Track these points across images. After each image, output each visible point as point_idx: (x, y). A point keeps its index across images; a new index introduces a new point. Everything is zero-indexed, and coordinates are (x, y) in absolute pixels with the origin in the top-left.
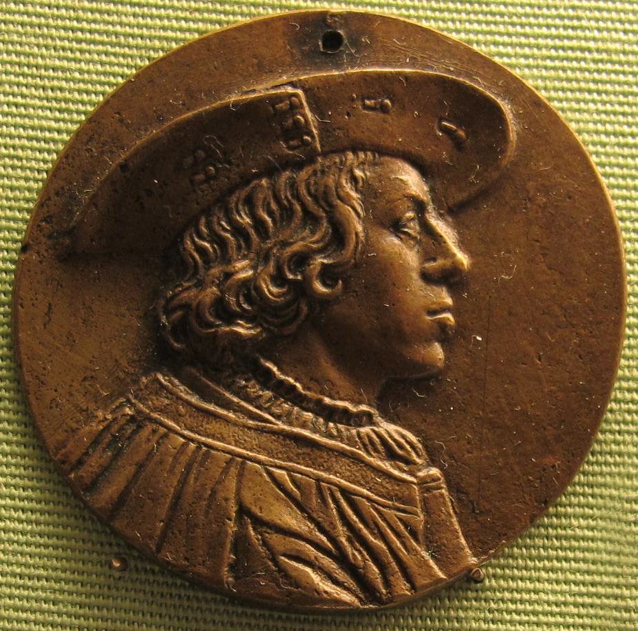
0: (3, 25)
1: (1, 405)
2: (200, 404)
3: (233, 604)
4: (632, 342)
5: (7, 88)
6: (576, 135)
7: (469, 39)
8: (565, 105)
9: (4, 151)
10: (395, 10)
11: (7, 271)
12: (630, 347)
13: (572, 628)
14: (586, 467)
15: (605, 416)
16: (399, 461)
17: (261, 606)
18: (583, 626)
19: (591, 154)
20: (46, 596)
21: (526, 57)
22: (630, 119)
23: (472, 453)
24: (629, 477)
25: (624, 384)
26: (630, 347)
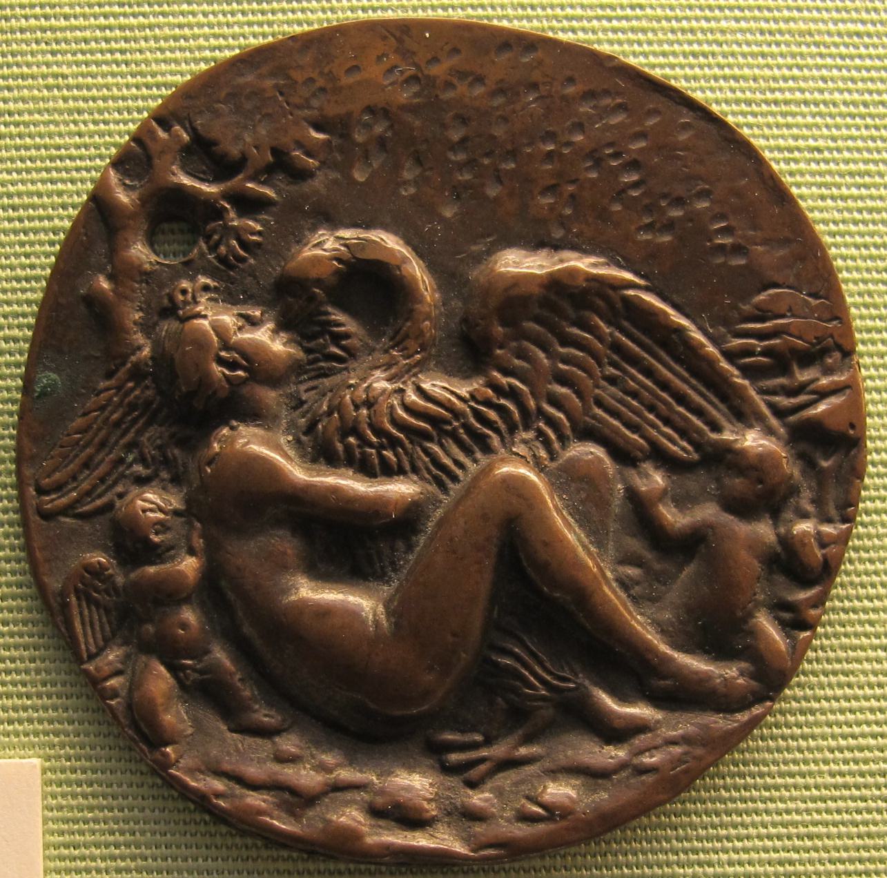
0: (3, 21)
2: (340, 597)
3: (266, 847)
4: (879, 444)
6: (807, 213)
7: (846, 782)
8: (750, 119)
10: (470, 11)
12: (878, 451)
13: (863, 876)
14: (806, 665)
16: (605, 691)
17: (284, 846)
18: (867, 873)
19: (824, 233)
20: (785, 870)
21: (854, 799)
22: (877, 603)
23: (396, 364)
26: (878, 451)
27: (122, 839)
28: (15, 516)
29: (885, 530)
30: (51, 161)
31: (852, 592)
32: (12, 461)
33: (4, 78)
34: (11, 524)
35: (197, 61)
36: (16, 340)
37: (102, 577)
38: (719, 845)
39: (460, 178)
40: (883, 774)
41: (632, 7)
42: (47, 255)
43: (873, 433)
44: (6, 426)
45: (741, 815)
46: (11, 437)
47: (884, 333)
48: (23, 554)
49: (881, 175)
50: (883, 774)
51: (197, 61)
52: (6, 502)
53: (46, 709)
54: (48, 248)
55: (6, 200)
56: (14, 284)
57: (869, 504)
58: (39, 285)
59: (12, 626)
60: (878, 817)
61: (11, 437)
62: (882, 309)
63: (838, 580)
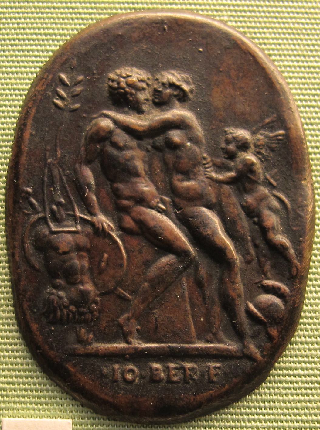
1: (1, 180)
9: (2, 143)
11: (5, 158)
24: (316, 14)
27: (18, 354)
28: (8, 284)
31: (262, 405)
32: (7, 262)
33: (2, 45)
34: (5, 287)
37: (173, 147)
39: (82, 287)
42: (26, 84)
45: (264, 403)
48: (12, 308)
53: (34, 384)
54: (27, 81)
55: (2, 132)
58: (22, 98)
60: (315, 405)
63: (296, 333)
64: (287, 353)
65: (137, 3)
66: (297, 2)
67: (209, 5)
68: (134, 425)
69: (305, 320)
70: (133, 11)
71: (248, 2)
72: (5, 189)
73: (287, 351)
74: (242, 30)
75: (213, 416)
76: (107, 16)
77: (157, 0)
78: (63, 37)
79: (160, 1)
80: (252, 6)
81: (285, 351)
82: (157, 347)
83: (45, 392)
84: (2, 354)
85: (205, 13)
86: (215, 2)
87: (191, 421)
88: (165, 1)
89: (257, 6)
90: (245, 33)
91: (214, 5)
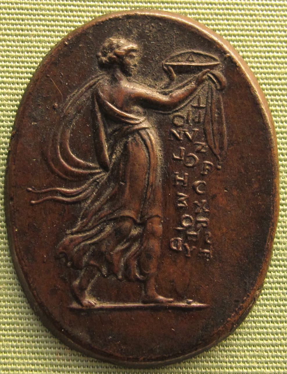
4: (284, 162)
5: (4, 32)
15: (276, 235)
25: (281, 229)
29: (286, 185)
30: (22, 42)
35: (70, 27)
36: (9, 116)
38: (231, 359)
40: (286, 42)
41: (207, 4)
43: (282, 202)
44: (2, 249)
46: (6, 154)
47: (285, 96)
48: (9, 258)
49: (285, 31)
50: (286, 42)
51: (70, 27)
52: (2, 257)
56: (9, 102)
57: (279, 246)
59: (4, 296)
61: (6, 154)
62: (285, 156)
64: (253, 313)
65: (154, 3)
66: (106, 2)
67: (237, 4)
68: (117, 366)
69: (268, 285)
70: (133, 9)
71: (277, 2)
72: (6, 160)
73: (252, 312)
74: (211, 27)
75: (187, 364)
76: (101, 14)
77: (204, 0)
78: (61, 33)
79: (214, 1)
80: (267, 5)
81: (251, 312)
82: (202, 306)
83: (31, 331)
84: (2, 298)
85: (169, 10)
86: (247, 2)
87: (163, 367)
88: (15, 1)
89: (87, 6)
90: (214, 30)
91: (246, 4)
